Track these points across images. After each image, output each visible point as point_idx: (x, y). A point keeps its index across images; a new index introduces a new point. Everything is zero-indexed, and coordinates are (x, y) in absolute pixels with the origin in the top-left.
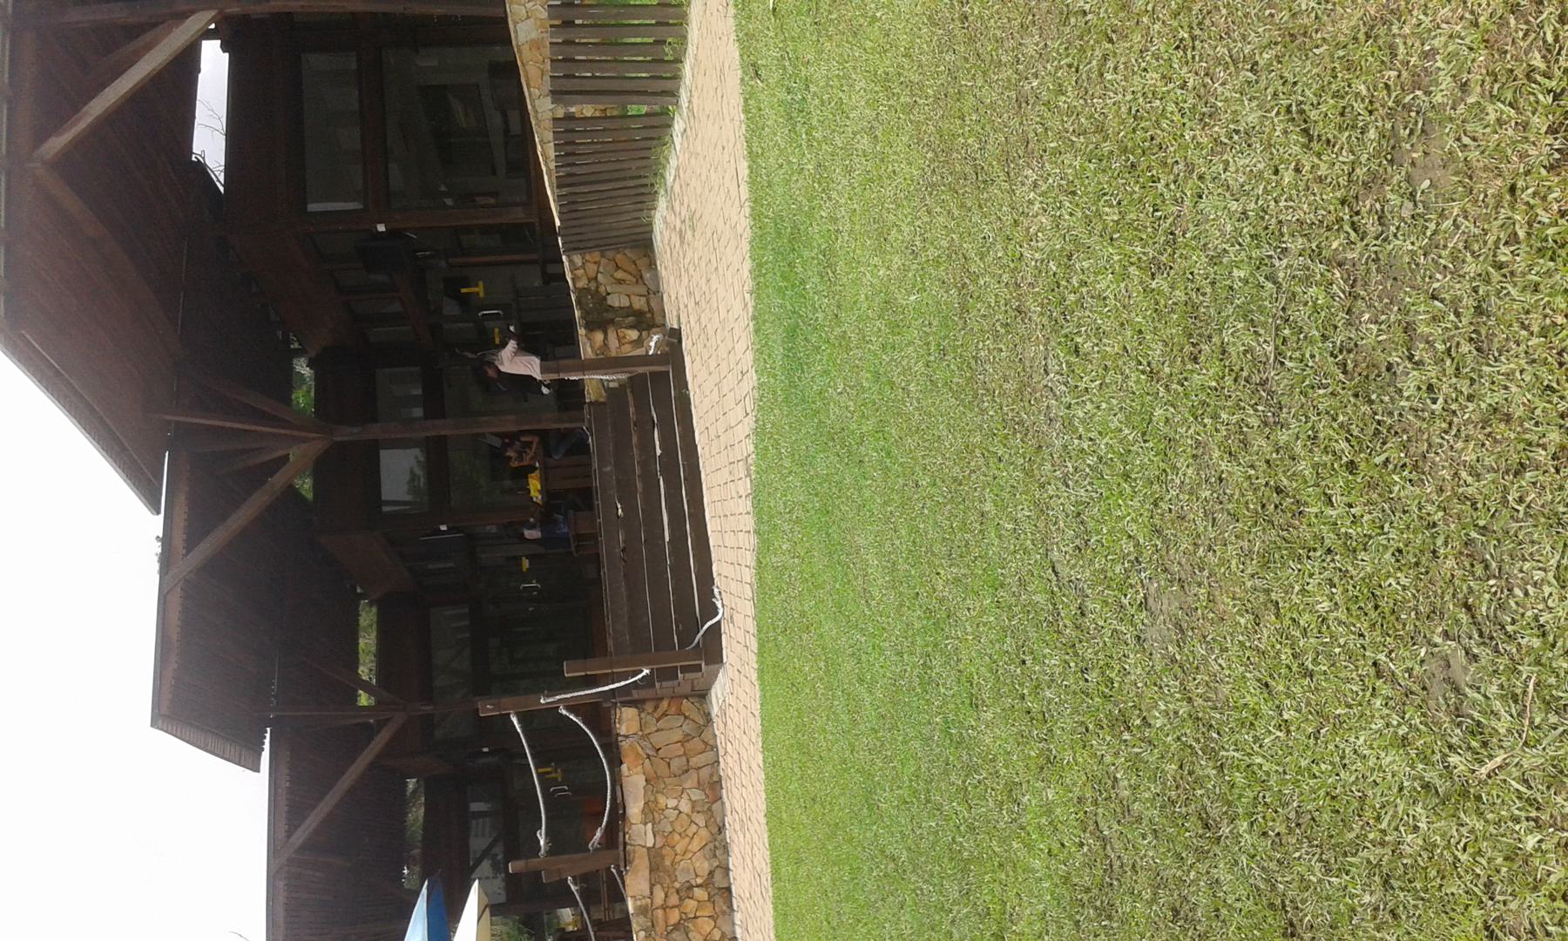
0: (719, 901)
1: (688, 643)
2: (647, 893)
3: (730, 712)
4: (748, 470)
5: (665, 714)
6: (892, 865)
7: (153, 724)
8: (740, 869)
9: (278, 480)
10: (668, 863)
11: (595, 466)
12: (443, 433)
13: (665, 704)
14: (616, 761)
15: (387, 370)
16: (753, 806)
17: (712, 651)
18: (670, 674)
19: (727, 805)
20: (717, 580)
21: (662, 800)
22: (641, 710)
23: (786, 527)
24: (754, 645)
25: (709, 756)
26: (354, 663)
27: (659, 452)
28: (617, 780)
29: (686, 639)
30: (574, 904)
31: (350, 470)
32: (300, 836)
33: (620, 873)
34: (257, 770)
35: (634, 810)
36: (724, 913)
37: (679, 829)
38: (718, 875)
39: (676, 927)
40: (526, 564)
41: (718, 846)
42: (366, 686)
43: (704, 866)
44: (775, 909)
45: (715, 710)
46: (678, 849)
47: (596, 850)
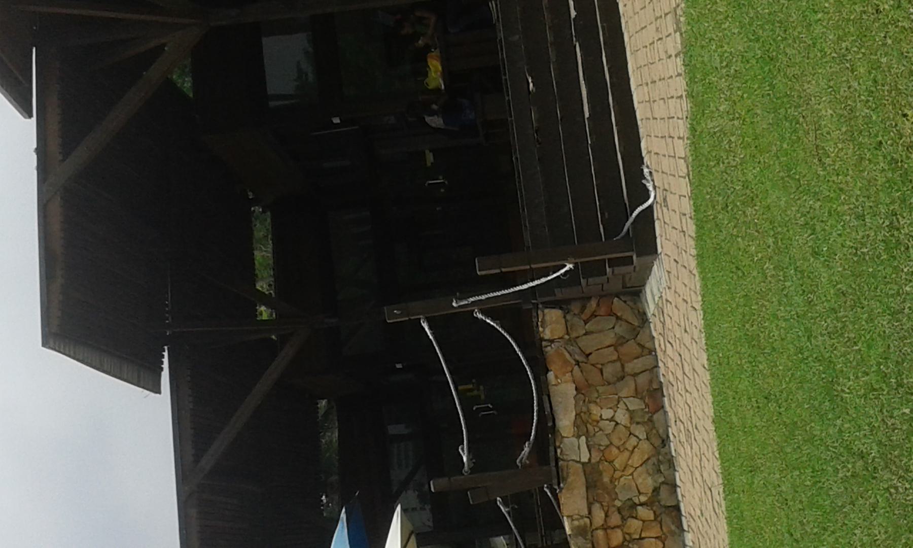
0: (667, 520)
1: (618, 235)
2: (586, 512)
3: (668, 309)
4: (678, 22)
5: (594, 315)
6: (860, 463)
7: (44, 345)
8: (689, 485)
10: (606, 479)
11: (501, 35)
13: (593, 303)
14: (541, 367)
16: (700, 414)
17: (644, 241)
18: (596, 269)
19: (671, 414)
20: (646, 160)
21: (595, 410)
22: (566, 312)
23: (723, 84)
24: (692, 229)
25: (646, 361)
26: (252, 278)
27: (573, 14)
29: (614, 227)
30: (507, 531)
32: (208, 462)
33: (553, 492)
34: (157, 389)
35: (565, 422)
36: (673, 533)
37: (616, 442)
38: (664, 493)
40: (430, 158)
41: (662, 461)
42: (264, 299)
43: (647, 483)
44: (730, 523)
45: (651, 309)
47: (524, 466)
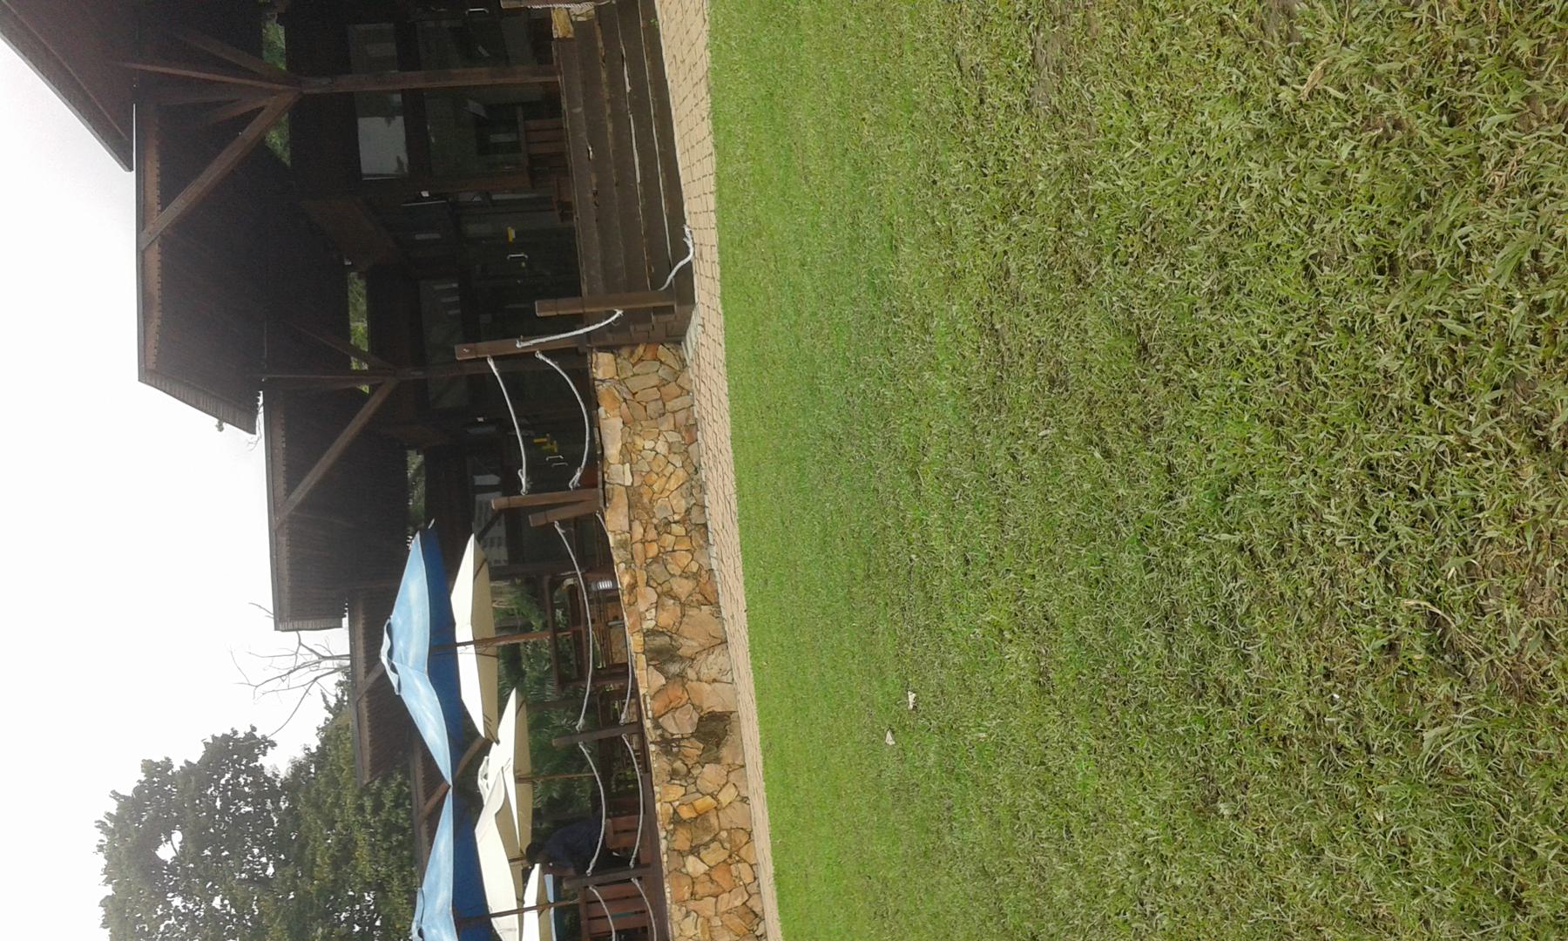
0: (697, 538)
3: (703, 352)
5: (641, 360)
7: (276, 629)
9: (249, 134)
10: (646, 500)
11: (565, 106)
12: (415, 86)
13: (640, 350)
14: (593, 403)
15: (361, 27)
17: (684, 292)
21: (639, 442)
25: (686, 400)
28: (594, 421)
29: (658, 281)
31: (326, 129)
32: (299, 495)
35: (613, 451)
36: (701, 547)
37: (656, 469)
38: (695, 513)
39: (655, 559)
41: (694, 485)
42: (361, 356)
43: (681, 504)
46: (655, 487)
47: (576, 488)
